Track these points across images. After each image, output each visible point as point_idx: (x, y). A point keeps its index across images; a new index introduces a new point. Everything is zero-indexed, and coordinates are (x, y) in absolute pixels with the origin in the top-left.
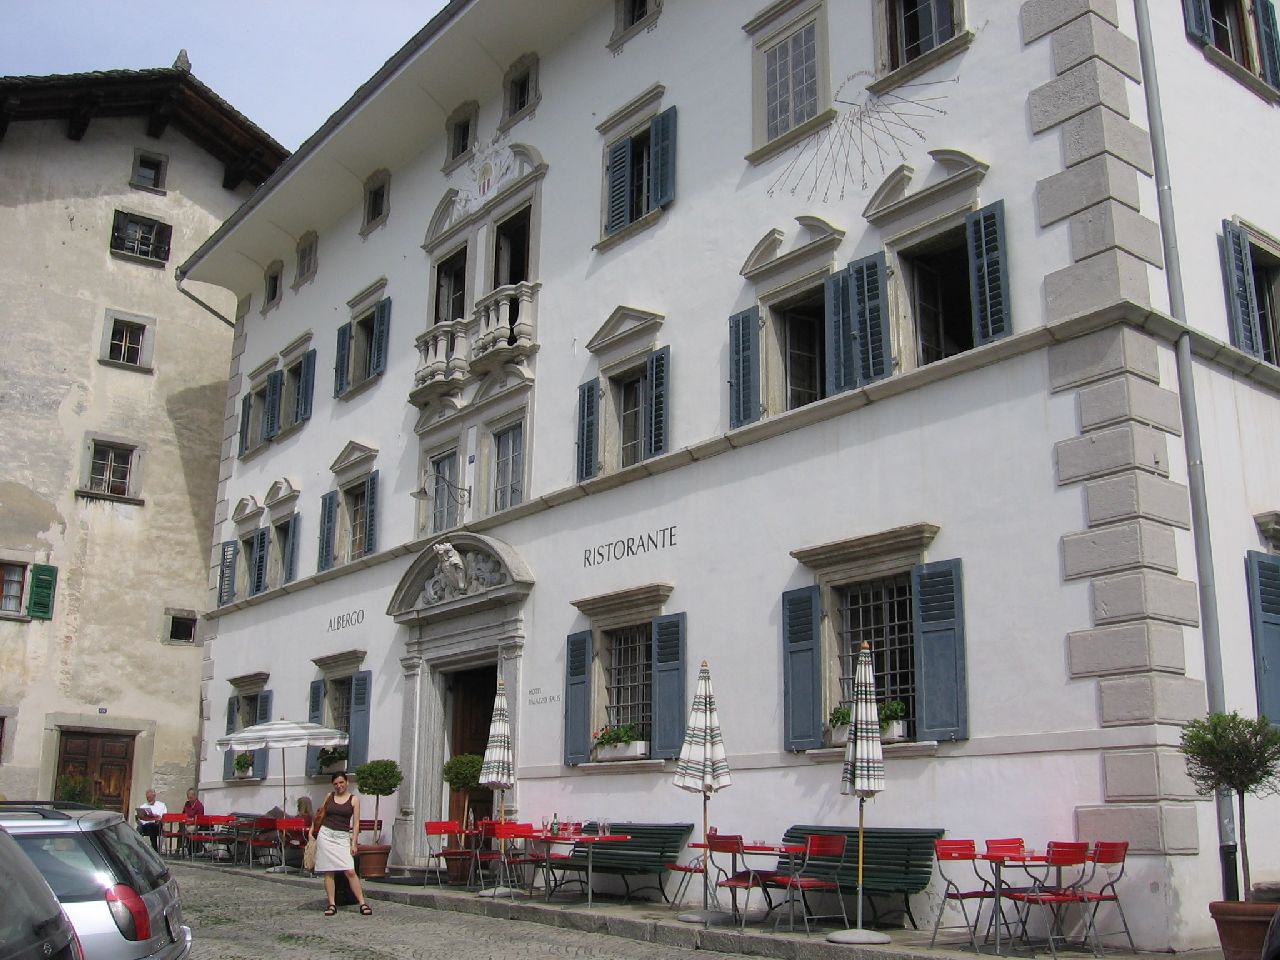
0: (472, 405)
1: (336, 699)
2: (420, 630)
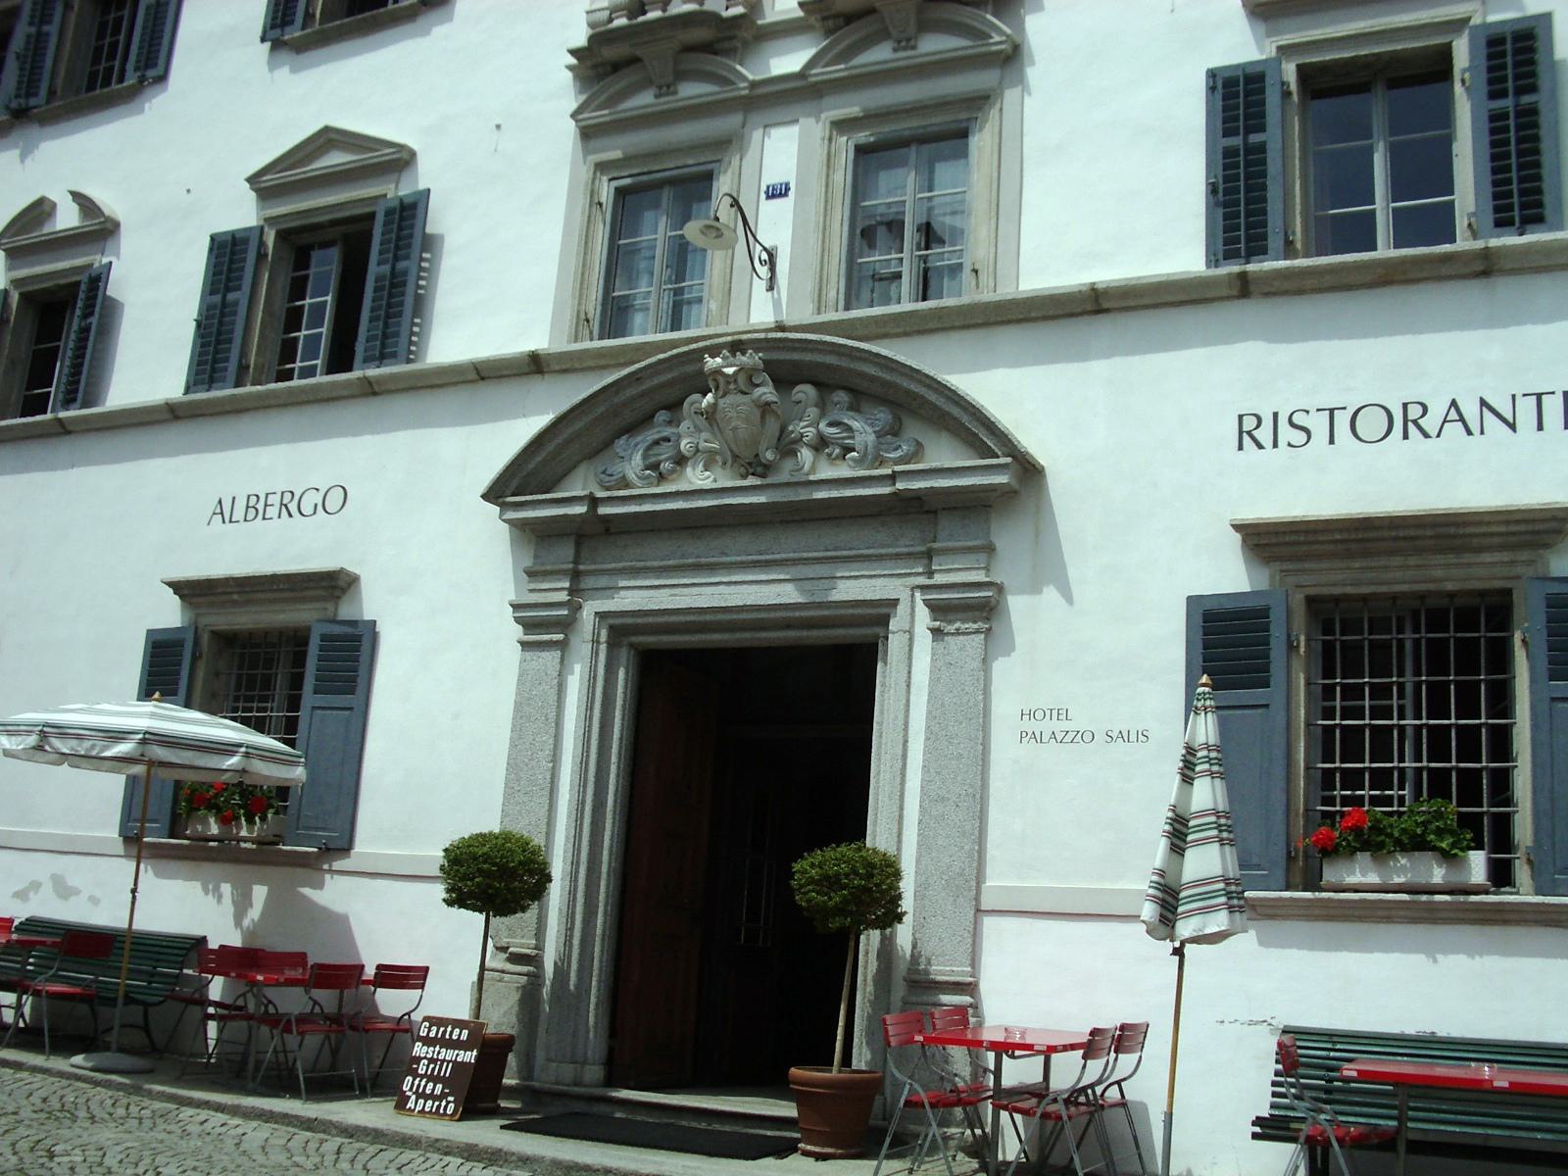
0: (801, 75)
1: (217, 674)
2: (578, 545)
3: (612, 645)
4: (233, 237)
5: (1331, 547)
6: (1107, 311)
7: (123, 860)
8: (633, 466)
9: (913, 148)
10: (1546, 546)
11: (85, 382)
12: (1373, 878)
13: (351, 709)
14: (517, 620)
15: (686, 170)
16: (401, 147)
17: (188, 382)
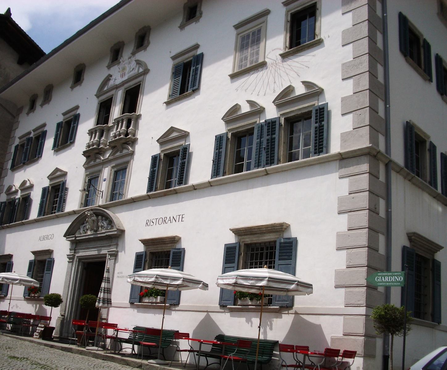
3: (79, 262)
4: (220, 136)
5: (150, 244)
6: (135, 202)
7: (130, 309)
8: (81, 231)
9: (121, 172)
10: (176, 243)
11: (183, 178)
12: (148, 301)
13: (49, 273)
14: (68, 258)
15: (96, 176)
16: (186, 132)
17: (212, 175)
